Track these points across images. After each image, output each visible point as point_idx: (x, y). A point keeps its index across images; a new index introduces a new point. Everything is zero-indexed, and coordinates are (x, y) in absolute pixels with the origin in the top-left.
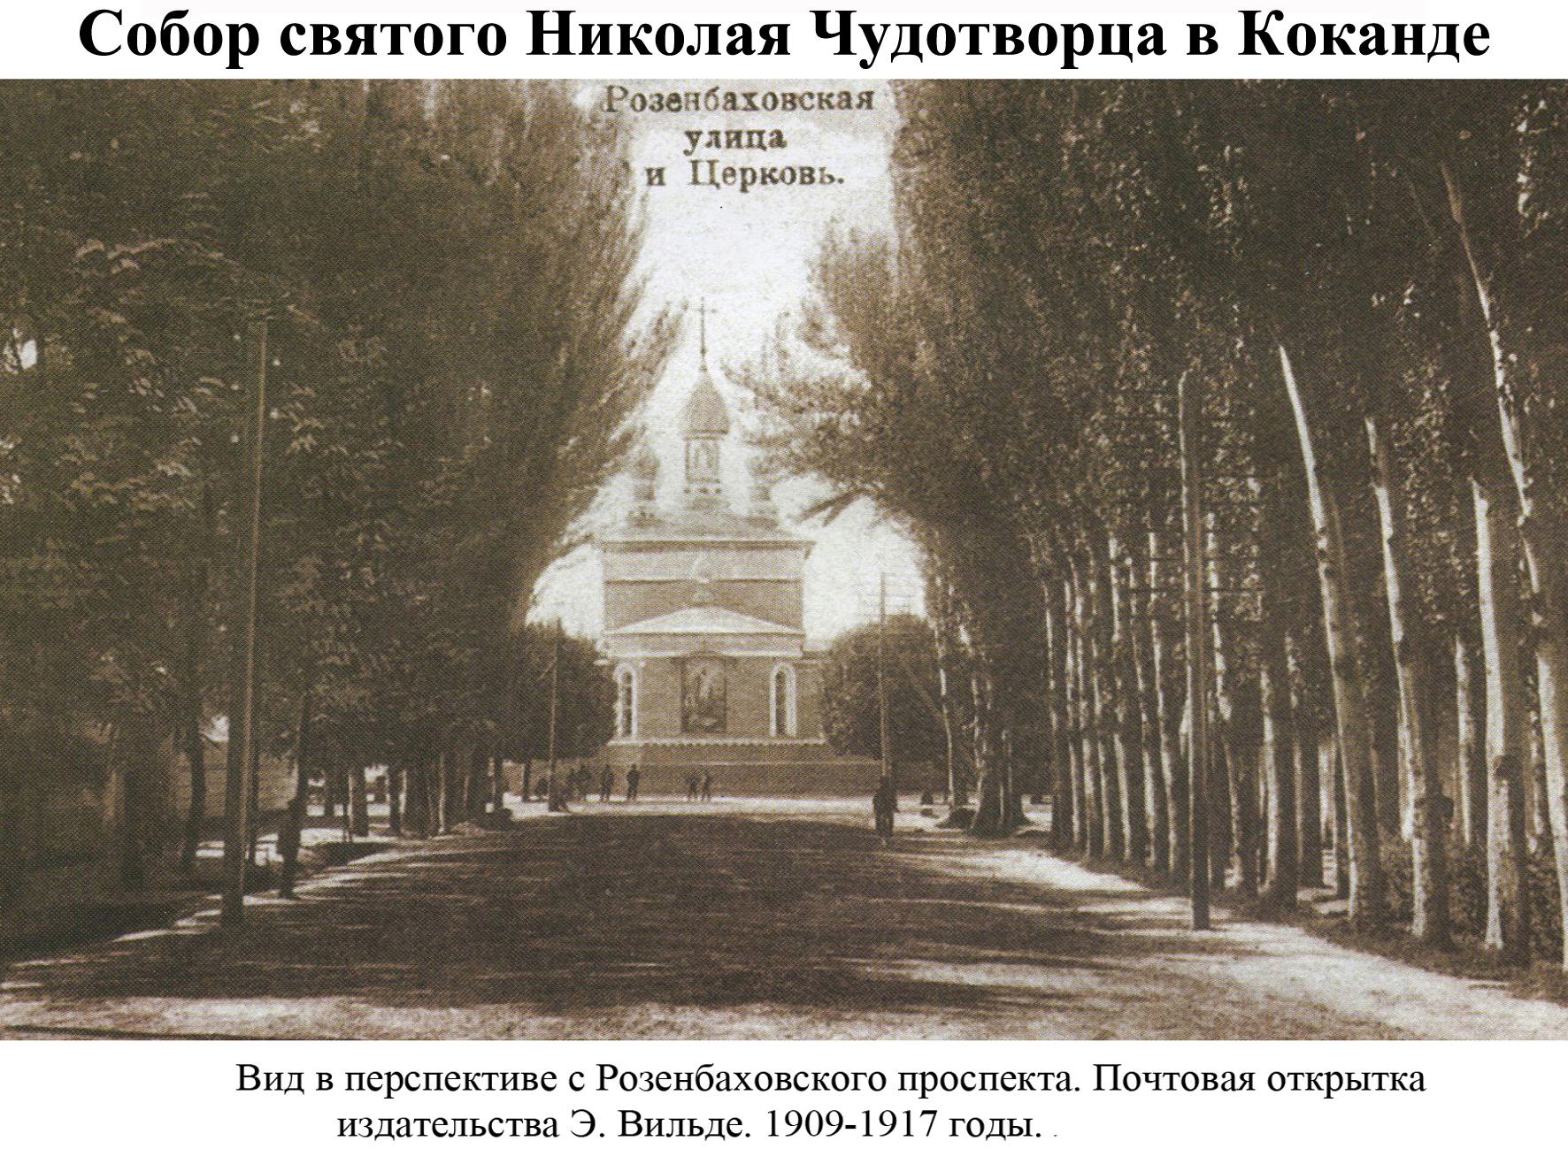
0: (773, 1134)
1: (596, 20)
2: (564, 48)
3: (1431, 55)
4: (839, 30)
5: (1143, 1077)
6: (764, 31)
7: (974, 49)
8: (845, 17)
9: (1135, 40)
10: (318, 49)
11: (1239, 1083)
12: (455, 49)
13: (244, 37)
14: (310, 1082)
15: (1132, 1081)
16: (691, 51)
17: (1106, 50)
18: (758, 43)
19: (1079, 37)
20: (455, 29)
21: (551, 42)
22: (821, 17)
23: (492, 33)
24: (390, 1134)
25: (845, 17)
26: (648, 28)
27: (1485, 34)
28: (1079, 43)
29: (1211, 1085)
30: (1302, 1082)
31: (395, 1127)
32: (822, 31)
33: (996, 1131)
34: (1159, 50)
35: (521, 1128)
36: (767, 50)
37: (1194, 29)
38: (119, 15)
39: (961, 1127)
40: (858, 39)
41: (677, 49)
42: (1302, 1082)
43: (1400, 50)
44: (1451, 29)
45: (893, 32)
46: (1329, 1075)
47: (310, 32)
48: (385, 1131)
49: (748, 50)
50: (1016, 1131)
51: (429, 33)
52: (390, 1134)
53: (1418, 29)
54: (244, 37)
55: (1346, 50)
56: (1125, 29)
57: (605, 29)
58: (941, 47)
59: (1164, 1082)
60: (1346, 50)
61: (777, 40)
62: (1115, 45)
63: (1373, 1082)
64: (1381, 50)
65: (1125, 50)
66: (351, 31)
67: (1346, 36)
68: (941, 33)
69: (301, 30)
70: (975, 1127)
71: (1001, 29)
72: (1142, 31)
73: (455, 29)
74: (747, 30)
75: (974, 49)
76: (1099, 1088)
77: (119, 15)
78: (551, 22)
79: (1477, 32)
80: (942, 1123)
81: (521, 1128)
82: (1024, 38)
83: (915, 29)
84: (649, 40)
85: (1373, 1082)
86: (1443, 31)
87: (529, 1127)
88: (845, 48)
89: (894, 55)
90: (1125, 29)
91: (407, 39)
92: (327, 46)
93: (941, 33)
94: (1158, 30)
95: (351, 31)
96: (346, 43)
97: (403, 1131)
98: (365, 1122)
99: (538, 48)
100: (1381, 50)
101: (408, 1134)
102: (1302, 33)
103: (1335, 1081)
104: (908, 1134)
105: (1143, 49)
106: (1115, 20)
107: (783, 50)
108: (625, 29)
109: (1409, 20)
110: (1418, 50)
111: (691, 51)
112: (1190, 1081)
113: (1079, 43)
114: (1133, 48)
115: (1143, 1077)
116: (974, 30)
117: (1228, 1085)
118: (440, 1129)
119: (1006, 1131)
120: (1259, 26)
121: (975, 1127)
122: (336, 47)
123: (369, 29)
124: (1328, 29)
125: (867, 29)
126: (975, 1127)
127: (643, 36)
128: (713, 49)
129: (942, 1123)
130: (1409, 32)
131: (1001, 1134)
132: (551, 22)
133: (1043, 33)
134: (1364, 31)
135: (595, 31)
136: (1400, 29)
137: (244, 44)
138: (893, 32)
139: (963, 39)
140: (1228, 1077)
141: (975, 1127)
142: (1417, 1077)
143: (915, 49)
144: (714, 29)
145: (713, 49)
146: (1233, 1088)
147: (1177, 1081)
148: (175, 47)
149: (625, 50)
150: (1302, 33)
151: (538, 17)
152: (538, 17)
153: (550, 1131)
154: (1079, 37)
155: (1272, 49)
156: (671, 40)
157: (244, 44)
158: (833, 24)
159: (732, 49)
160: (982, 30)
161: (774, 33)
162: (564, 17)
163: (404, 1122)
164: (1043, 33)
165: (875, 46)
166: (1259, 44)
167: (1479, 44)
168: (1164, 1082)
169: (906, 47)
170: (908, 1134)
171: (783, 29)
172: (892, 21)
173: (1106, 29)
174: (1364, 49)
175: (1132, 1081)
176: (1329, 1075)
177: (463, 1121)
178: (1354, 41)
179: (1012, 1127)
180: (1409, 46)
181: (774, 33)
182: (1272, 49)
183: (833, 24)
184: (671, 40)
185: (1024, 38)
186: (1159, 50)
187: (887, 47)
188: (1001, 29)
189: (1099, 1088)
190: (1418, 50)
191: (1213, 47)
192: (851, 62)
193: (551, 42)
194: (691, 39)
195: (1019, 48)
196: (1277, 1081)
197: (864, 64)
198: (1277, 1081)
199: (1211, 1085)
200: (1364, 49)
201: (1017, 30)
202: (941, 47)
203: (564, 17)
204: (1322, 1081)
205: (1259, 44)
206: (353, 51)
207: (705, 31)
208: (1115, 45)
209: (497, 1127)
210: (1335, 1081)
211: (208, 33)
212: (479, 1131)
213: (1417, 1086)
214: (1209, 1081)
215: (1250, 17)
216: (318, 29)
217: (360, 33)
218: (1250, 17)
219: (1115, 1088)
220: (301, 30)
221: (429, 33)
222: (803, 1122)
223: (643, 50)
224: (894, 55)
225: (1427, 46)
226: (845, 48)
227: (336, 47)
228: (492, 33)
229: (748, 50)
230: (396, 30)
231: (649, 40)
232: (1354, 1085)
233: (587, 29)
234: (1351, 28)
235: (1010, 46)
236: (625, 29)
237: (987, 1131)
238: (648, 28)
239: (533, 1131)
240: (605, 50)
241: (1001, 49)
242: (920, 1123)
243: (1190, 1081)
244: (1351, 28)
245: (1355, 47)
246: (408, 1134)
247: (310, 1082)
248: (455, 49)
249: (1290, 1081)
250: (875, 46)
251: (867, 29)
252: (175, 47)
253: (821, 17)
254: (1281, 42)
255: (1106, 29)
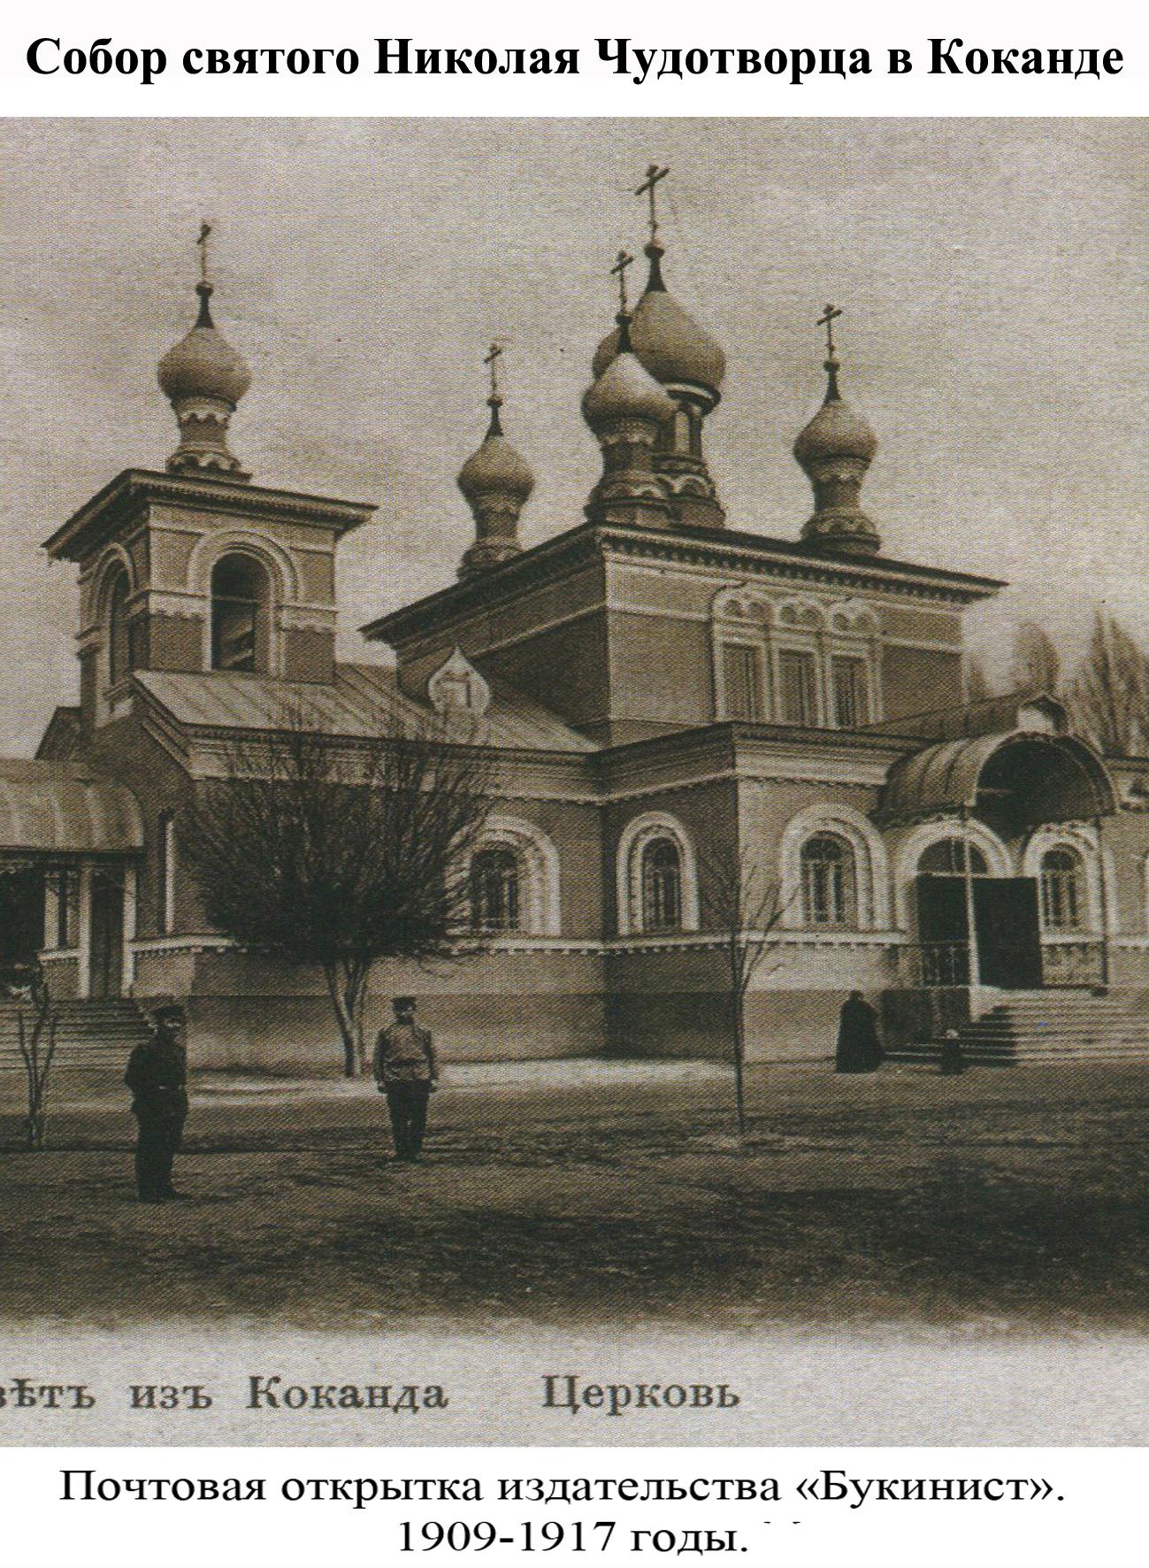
0: (407, 1548)
1: (428, 47)
2: (403, 68)
3: (1078, 73)
4: (617, 53)
5: (123, 1486)
6: (559, 55)
7: (722, 69)
8: (622, 44)
9: (847, 62)
10: (212, 69)
11: (244, 1491)
12: (319, 69)
13: (154, 58)
14: (880, 61)
15: (109, 1490)
16: (502, 70)
17: (825, 69)
18: (554, 64)
19: (804, 59)
20: (319, 54)
21: (393, 63)
22: (603, 44)
23: (347, 57)
24: (564, 1497)
25: (622, 44)
26: (469, 53)
27: (1120, 57)
28: (804, 64)
29: (209, 1494)
30: (326, 1490)
31: (571, 1489)
32: (604, 55)
33: (691, 1544)
34: (866, 70)
35: (732, 1490)
36: (561, 70)
37: (894, 53)
38: (57, 43)
39: (646, 1541)
40: (632, 62)
41: (491, 69)
42: (326, 1490)
43: (1053, 70)
44: (1093, 54)
45: (659, 56)
46: (359, 1483)
47: (206, 55)
48: (559, 1493)
49: (546, 70)
50: (715, 1545)
51: (298, 57)
52: (564, 1497)
53: (1067, 53)
54: (154, 58)
55: (1012, 69)
56: (839, 53)
57: (435, 54)
58: (697, 66)
59: (150, 1490)
60: (1012, 69)
61: (569, 62)
62: (832, 66)
63: (416, 1490)
64: (1038, 70)
65: (839, 69)
66: (238, 55)
67: (1011, 59)
68: (697, 56)
69: (199, 54)
70: (664, 1541)
71: (743, 53)
72: (853, 55)
73: (319, 54)
74: (546, 54)
75: (722, 69)
76: (67, 1496)
77: (57, 43)
78: (393, 48)
79: (1113, 55)
80: (622, 1537)
81: (732, 1490)
82: (761, 60)
83: (676, 53)
84: (470, 62)
85: (416, 1490)
86: (1087, 55)
87: (741, 1489)
88: (622, 69)
89: (660, 73)
90: (839, 53)
91: (281, 61)
92: (219, 66)
93: (697, 56)
94: (865, 54)
95: (238, 55)
96: (234, 64)
97: (581, 1494)
98: (535, 1484)
99: (383, 68)
100: (1038, 70)
101: (588, 1497)
102: (977, 57)
103: (367, 1490)
104: (579, 1548)
105: (853, 69)
106: (832, 46)
107: (574, 70)
108: (451, 53)
109: (1060, 46)
110: (1067, 69)
111: (502, 70)
112: (183, 1490)
113: (804, 64)
114: (846, 68)
115: (123, 1486)
116: (722, 54)
117: (232, 1494)
118: (628, 1492)
119: (703, 1544)
120: (944, 51)
121: (664, 1541)
122: (226, 68)
123: (252, 53)
124: (998, 53)
125: (639, 53)
126: (664, 1541)
127: (465, 59)
128: (520, 69)
129: (622, 1537)
130: (1060, 56)
131: (697, 1548)
132: (393, 48)
133: (776, 57)
134: (1026, 55)
135: (428, 55)
136: (1053, 53)
137: (154, 64)
138: (659, 56)
139: (713, 61)
140: (232, 1484)
141: (664, 1541)
142: (472, 1484)
143: (676, 69)
144: (520, 54)
145: (520, 69)
146: (238, 1497)
147: (167, 1490)
148: (101, 66)
149: (451, 70)
150: (977, 57)
151: (383, 44)
152: (383, 44)
153: (769, 1494)
154: (804, 59)
155: (954, 69)
156: (486, 62)
157: (154, 64)
158: (613, 50)
159: (534, 69)
160: (728, 54)
161: (567, 56)
162: (403, 44)
163: (582, 1484)
164: (776, 57)
165: (645, 66)
166: (944, 65)
167: (1115, 65)
168: (150, 1490)
169: (669, 67)
170: (579, 1548)
171: (574, 53)
172: (659, 48)
173: (825, 53)
174: (1026, 69)
175: (109, 1490)
176: (359, 1483)
177: (659, 1483)
178: (1018, 62)
179: (710, 1540)
180: (1060, 66)
181: (567, 56)
182: (954, 69)
183: (613, 50)
184: (486, 62)
185: (761, 60)
186: (866, 70)
187: (655, 67)
188: (743, 53)
189: (67, 1496)
190: (1067, 69)
191: (908, 68)
192: (626, 79)
193: (393, 63)
194: (501, 62)
195: (757, 68)
196: (293, 1489)
197: (637, 81)
198: (293, 1489)
199: (209, 1494)
200: (1026, 69)
201: (756, 54)
202: (697, 66)
203: (403, 44)
204: (352, 1490)
205: (944, 65)
206: (240, 70)
207: (513, 55)
208: (832, 66)
209: (700, 1489)
210: (367, 1490)
211: (127, 56)
212: (677, 1494)
213: (471, 1494)
214: (208, 1489)
215: (936, 44)
216: (212, 53)
217: (245, 56)
218: (936, 44)
219: (88, 1496)
220: (199, 54)
221: (298, 57)
222: (445, 1535)
223: (465, 70)
224: (660, 73)
225: (1074, 67)
226: (622, 69)
227: (226, 68)
228: (347, 57)
229: (546, 70)
230: (273, 54)
231: (470, 62)
232: (392, 1494)
233: (421, 53)
234: (1015, 53)
235: (750, 66)
236: (451, 53)
237: (678, 1545)
238: (469, 53)
239: (747, 1494)
240: (435, 70)
241: (743, 69)
242: (593, 1538)
243: (183, 1490)
244: (1015, 53)
245: (1018, 67)
246: (588, 1497)
247: (880, 61)
248: (319, 69)
249: (310, 1490)
250: (645, 66)
251: (639, 53)
252: (101, 66)
253: (603, 44)
254: (961, 63)
255: (825, 53)
